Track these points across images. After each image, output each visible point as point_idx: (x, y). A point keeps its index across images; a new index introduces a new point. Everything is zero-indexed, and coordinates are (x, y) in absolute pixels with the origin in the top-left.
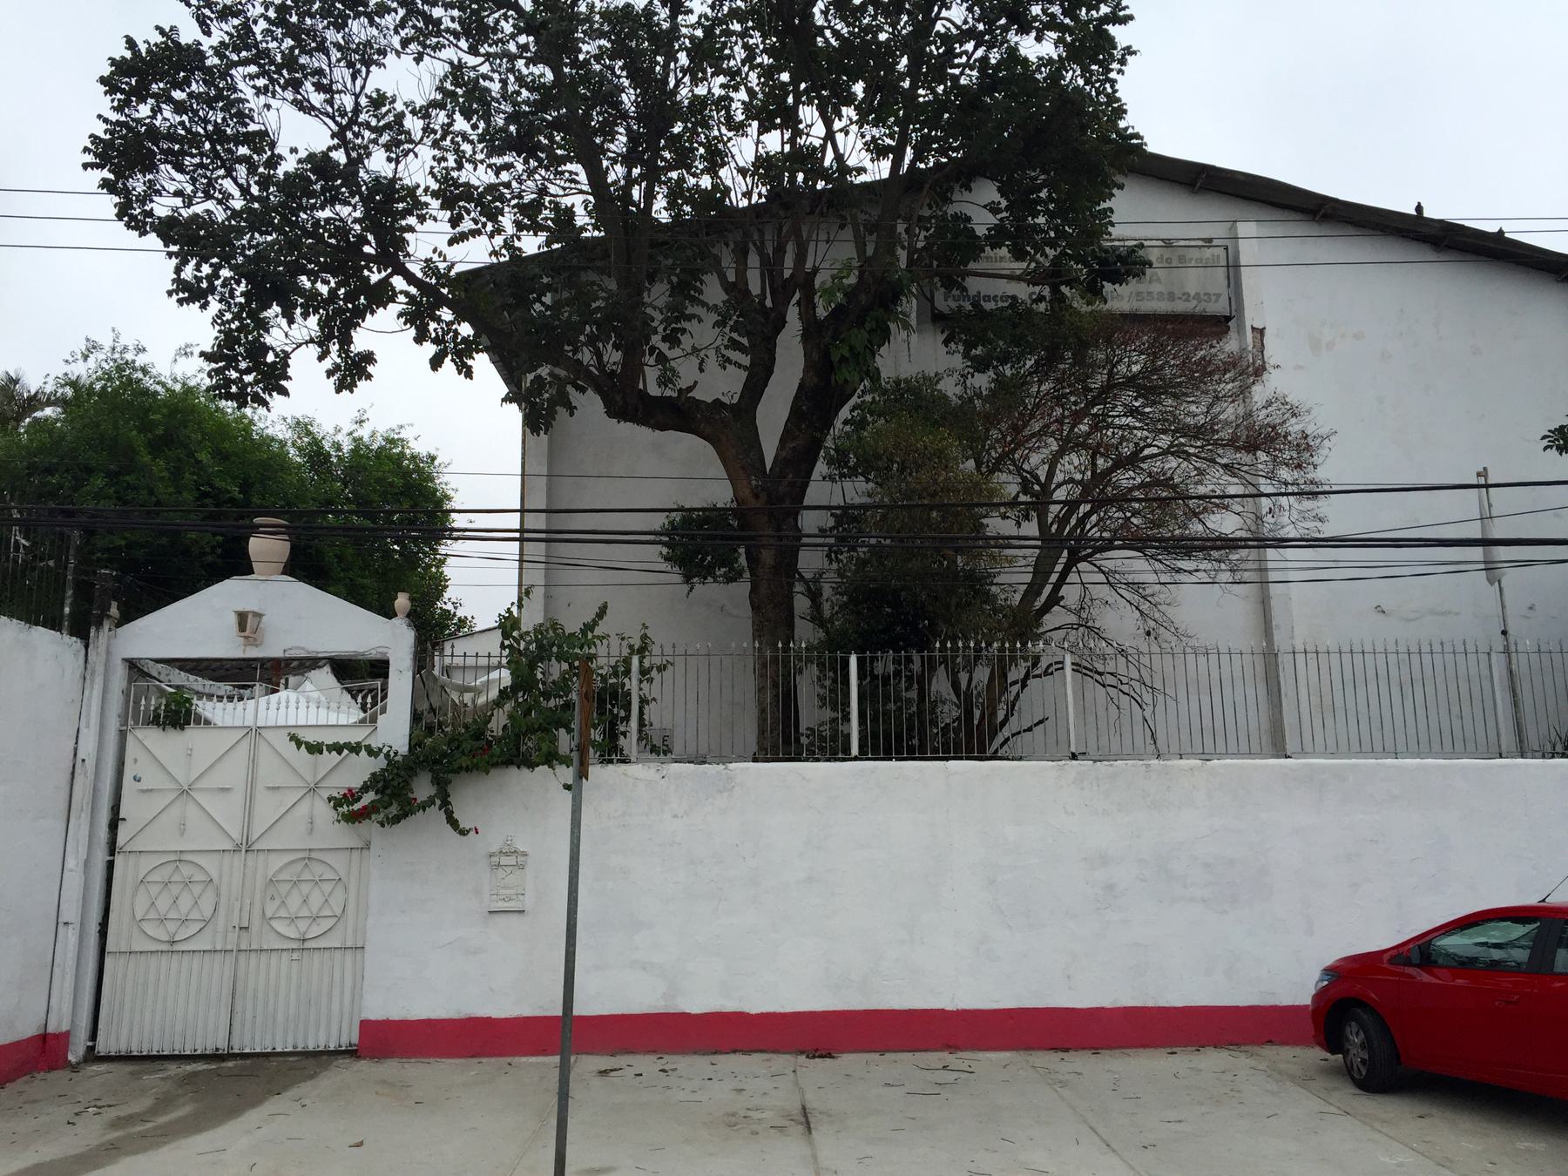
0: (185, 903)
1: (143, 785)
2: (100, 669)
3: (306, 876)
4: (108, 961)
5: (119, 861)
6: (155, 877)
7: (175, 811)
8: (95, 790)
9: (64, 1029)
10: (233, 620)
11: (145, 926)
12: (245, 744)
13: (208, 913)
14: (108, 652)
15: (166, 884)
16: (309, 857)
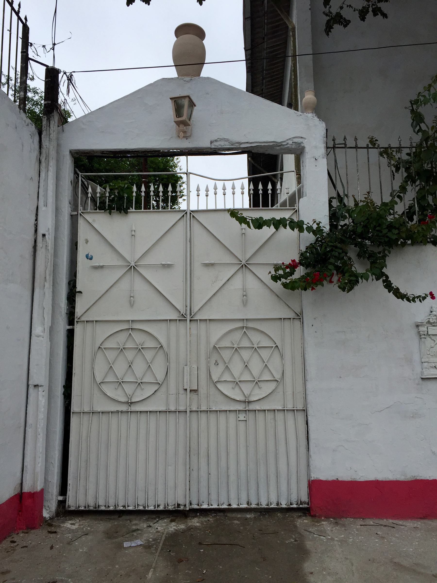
0: (139, 367)
1: (95, 262)
2: (53, 153)
3: (245, 343)
4: (74, 420)
5: (78, 329)
6: (109, 344)
7: (125, 285)
8: (55, 266)
9: (39, 489)
10: (169, 110)
11: (104, 388)
12: (181, 227)
13: (160, 377)
14: (59, 145)
15: (122, 350)
16: (245, 326)
